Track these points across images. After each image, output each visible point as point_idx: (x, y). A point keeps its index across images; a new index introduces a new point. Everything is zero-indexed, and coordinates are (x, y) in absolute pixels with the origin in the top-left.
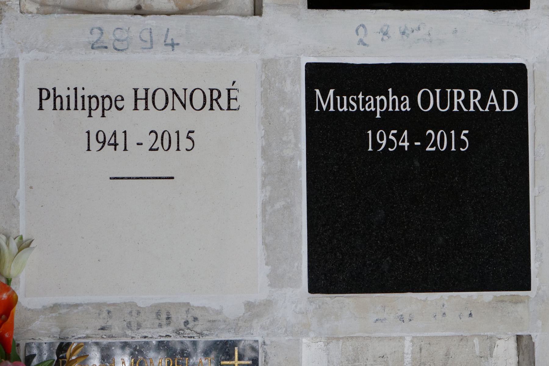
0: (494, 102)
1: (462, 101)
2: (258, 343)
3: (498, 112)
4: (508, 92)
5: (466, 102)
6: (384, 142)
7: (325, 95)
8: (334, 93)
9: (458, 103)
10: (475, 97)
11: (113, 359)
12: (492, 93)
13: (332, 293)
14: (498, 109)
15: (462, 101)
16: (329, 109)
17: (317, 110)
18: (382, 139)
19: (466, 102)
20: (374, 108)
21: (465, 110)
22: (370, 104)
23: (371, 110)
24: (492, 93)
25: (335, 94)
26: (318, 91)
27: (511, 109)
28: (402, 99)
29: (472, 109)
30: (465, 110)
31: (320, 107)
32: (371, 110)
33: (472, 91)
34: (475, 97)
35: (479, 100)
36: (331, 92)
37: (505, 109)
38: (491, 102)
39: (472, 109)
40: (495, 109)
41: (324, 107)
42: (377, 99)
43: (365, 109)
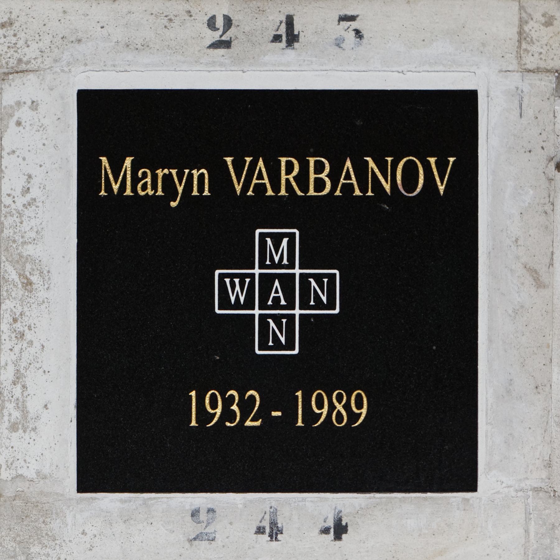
0: (263, 179)
1: (294, 178)
2: (271, 519)
3: (271, 196)
4: (316, 162)
5: (302, 179)
6: (219, 411)
7: (116, 168)
8: (133, 162)
9: (287, 180)
10: (289, 171)
11: (258, 499)
12: (348, 164)
13: (199, 491)
14: (270, 193)
15: (294, 178)
16: (125, 191)
17: (103, 193)
18: (214, 405)
19: (302, 179)
20: (152, 190)
21: (299, 193)
22: (146, 184)
23: (147, 194)
24: (348, 164)
25: (135, 168)
26: (104, 160)
27: (178, 193)
28: (140, 174)
29: (283, 192)
30: (299, 193)
31: (109, 188)
32: (147, 194)
33: (312, 160)
34: (289, 171)
35: (296, 176)
36: (128, 161)
37: (312, 192)
38: (345, 179)
39: (283, 192)
40: (354, 191)
41: (116, 187)
42: (157, 174)
43: (223, 395)
